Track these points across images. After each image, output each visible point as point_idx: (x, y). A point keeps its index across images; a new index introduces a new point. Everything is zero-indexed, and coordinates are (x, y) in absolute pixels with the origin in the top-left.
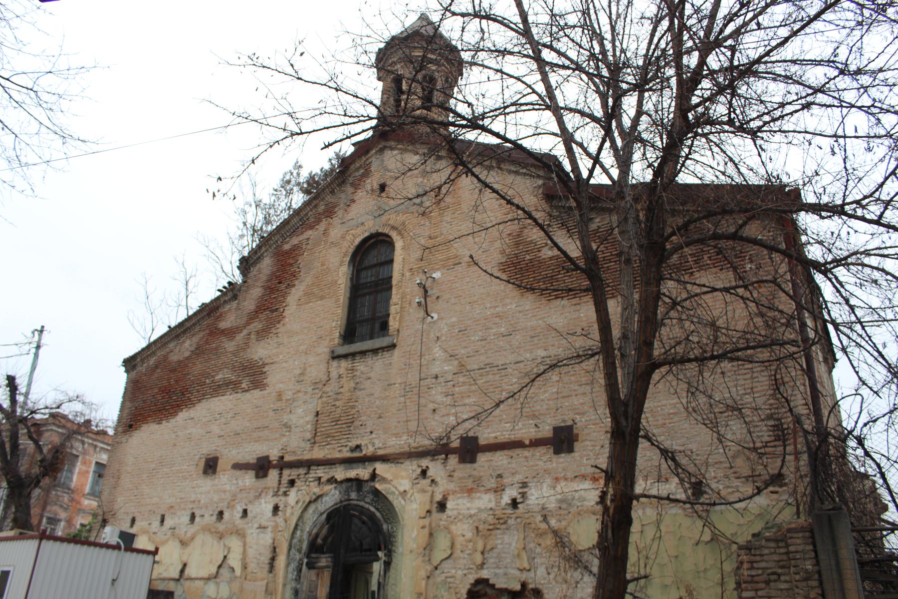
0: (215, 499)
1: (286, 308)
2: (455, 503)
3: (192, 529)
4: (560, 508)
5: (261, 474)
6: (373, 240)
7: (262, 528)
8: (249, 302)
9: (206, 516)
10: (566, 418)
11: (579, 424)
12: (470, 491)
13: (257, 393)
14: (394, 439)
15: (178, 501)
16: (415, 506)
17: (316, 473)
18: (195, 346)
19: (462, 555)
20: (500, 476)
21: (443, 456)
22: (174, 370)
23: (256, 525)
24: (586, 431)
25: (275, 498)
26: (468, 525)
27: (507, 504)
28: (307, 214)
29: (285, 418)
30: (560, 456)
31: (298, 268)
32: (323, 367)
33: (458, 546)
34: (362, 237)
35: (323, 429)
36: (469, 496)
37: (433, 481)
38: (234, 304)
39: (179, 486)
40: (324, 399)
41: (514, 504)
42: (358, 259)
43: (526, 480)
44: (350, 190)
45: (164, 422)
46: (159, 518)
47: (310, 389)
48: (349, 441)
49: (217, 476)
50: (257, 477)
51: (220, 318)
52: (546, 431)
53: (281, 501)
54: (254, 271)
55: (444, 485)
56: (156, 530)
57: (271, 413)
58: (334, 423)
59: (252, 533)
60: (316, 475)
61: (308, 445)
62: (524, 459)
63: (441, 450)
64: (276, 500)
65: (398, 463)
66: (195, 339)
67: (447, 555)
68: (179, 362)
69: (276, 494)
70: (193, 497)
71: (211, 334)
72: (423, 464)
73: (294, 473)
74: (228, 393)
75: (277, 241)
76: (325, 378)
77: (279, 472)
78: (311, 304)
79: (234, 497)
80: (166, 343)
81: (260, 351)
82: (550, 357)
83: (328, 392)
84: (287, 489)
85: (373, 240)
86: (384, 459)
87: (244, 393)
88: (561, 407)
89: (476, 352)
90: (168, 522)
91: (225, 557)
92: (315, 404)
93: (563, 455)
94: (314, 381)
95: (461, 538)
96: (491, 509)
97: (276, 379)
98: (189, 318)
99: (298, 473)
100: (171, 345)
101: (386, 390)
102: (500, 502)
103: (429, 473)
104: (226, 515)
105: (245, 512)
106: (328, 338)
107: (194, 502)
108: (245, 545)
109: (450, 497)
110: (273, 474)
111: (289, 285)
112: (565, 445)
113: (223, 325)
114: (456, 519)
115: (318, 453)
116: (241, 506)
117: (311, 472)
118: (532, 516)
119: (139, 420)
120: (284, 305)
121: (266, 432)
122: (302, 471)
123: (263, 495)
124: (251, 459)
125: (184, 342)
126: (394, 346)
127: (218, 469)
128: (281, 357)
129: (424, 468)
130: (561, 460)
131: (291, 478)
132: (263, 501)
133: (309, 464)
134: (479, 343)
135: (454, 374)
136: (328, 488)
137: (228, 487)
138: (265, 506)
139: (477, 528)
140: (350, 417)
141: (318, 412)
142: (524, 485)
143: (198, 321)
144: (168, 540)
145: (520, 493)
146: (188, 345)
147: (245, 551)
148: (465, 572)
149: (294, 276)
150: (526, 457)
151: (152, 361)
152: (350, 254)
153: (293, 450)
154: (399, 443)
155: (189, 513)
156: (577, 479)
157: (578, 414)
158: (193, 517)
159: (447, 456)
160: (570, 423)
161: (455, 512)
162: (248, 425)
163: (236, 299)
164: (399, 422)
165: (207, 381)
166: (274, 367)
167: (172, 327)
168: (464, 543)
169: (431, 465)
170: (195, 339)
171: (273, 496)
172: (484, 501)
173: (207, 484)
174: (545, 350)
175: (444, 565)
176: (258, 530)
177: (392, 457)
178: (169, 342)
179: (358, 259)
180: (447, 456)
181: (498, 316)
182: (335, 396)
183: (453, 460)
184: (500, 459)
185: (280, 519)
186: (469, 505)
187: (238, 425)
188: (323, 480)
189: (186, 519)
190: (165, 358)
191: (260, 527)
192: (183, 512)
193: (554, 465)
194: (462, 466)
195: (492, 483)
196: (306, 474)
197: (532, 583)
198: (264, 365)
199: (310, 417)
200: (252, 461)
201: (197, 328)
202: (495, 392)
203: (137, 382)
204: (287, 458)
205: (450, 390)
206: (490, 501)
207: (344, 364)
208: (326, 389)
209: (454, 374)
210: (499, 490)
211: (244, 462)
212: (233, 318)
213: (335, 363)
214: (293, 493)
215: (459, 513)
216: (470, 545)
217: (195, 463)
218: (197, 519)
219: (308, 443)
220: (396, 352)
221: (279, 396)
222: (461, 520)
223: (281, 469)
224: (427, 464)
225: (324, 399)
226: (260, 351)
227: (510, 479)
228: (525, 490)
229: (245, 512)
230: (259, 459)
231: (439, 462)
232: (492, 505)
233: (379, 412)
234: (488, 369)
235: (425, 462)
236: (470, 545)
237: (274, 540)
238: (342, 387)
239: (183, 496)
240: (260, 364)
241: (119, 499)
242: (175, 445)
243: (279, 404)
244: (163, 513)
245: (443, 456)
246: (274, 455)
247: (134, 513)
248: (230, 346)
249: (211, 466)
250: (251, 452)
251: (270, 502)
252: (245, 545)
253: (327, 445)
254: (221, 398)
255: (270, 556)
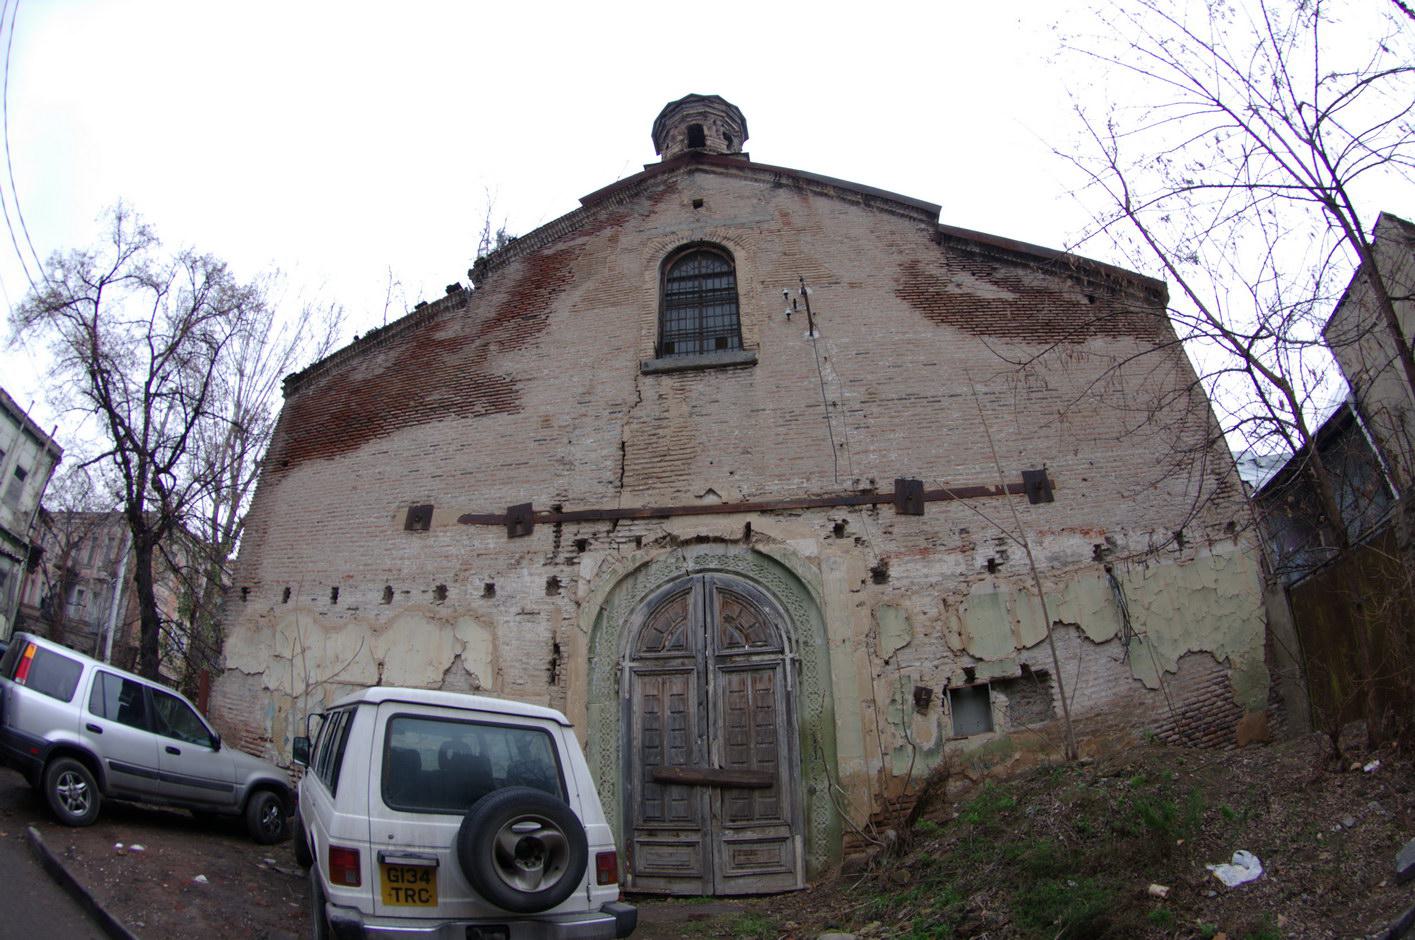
0: (430, 568)
1: (551, 315)
2: (903, 568)
3: (388, 612)
4: (1053, 567)
5: (519, 529)
6: (691, 250)
7: (528, 614)
8: (485, 310)
9: (413, 592)
10: (1034, 462)
11: (1051, 470)
12: (924, 552)
13: (503, 418)
14: (777, 482)
15: (361, 568)
16: (837, 575)
17: (630, 530)
18: (393, 361)
19: (926, 640)
20: (963, 531)
21: (870, 506)
22: (356, 391)
23: (515, 610)
24: (1062, 478)
25: (548, 568)
26: (929, 599)
27: (983, 567)
28: (581, 221)
29: (561, 451)
30: (1038, 505)
31: (570, 273)
32: (629, 385)
33: (919, 630)
34: (678, 244)
35: (636, 467)
36: (924, 558)
37: (857, 540)
38: (461, 312)
39: (363, 546)
40: (634, 426)
41: (992, 566)
42: (669, 267)
43: (1002, 536)
44: (647, 204)
45: (338, 457)
46: (329, 592)
47: (606, 413)
48: (690, 485)
49: (431, 534)
50: (512, 535)
51: (437, 327)
52: (1014, 476)
53: (564, 574)
54: (492, 277)
55: (879, 546)
56: (325, 610)
57: (533, 445)
58: (659, 459)
59: (507, 622)
60: (632, 534)
61: (611, 490)
62: (992, 509)
63: (865, 499)
64: (552, 571)
65: (791, 515)
66: (393, 354)
67: (905, 644)
68: (366, 381)
69: (551, 562)
70: (388, 563)
71: (422, 345)
72: (836, 517)
73: (585, 531)
74: (450, 419)
75: (532, 246)
76: (634, 398)
77: (1184, 343)
78: (596, 311)
79: (466, 567)
80: (348, 359)
81: (504, 365)
82: (994, 393)
83: (641, 417)
84: (574, 554)
85: (691, 250)
86: (764, 510)
87: (478, 418)
88: (1025, 450)
89: (890, 379)
90: (345, 599)
91: (458, 656)
92: (614, 433)
93: (1042, 504)
94: (610, 403)
95: (922, 617)
96: (961, 574)
97: (536, 400)
98: (386, 329)
99: (593, 530)
100: (355, 363)
101: (749, 417)
102: (972, 565)
103: (849, 529)
104: (453, 593)
105: (490, 589)
106: (632, 349)
107: (390, 570)
108: (495, 638)
109: (893, 562)
110: (543, 534)
111: (554, 290)
112: (1042, 492)
113: (440, 335)
114: (909, 592)
115: (627, 501)
116: (481, 580)
117: (618, 528)
118: (1021, 580)
119: (299, 456)
120: (547, 311)
121: (524, 471)
122: (603, 527)
123: (525, 563)
124: (499, 509)
125: (375, 357)
126: (754, 363)
127: (433, 522)
128: (546, 372)
129: (840, 522)
130: (1041, 511)
131: (579, 537)
132: (525, 572)
133: (615, 517)
134: (892, 369)
135: (862, 402)
136: (655, 552)
137: (453, 550)
138: (531, 581)
139: (944, 600)
140: (688, 451)
141: (623, 443)
142: (1001, 541)
143: (401, 331)
144: (346, 625)
145: (998, 552)
146: (381, 361)
147: (495, 647)
148: (936, 663)
149: (564, 281)
150: (995, 507)
151: (323, 382)
152: (661, 259)
153: (582, 497)
154: (786, 487)
155: (383, 586)
156: (1065, 533)
157: (1048, 459)
158: (389, 593)
159: (874, 505)
160: (1040, 468)
161: (905, 582)
162: (488, 460)
163: (463, 307)
164: (781, 459)
165: (412, 403)
166: (531, 384)
167: (361, 337)
168: (928, 623)
169: (850, 518)
170: (393, 354)
171: (545, 565)
172: (948, 565)
173: (414, 545)
174: (986, 385)
175: (901, 656)
176: (518, 618)
177: (780, 506)
178: (353, 357)
179: (669, 267)
180: (874, 505)
181: (909, 342)
182: (657, 423)
183: (887, 512)
184: (958, 509)
185: (563, 601)
186: (925, 571)
187: (469, 461)
188: (644, 541)
189: (378, 596)
190: (343, 377)
191: (523, 612)
192: (371, 585)
193: (1034, 516)
194: (903, 518)
195: (956, 541)
196: (608, 532)
197: (1033, 665)
198: (513, 382)
199: (614, 450)
200: (497, 512)
201: (398, 340)
202: (930, 427)
203: (299, 407)
204: (567, 508)
205: (862, 422)
206: (957, 564)
207: (667, 382)
208: (636, 412)
209: (862, 402)
210: (967, 549)
211: (485, 513)
212: (457, 327)
213: (649, 380)
214: (588, 563)
215: (912, 583)
216: (938, 625)
217: (391, 513)
218: (397, 597)
219: (610, 486)
220: (758, 370)
221: (546, 422)
222: (916, 592)
223: (558, 525)
224: (844, 517)
225: (634, 426)
226: (504, 365)
227: (981, 534)
228: (1003, 548)
229: (490, 589)
230: (511, 510)
231: (865, 514)
232: (962, 568)
233: (742, 445)
234: (913, 400)
235: (840, 514)
236: (938, 625)
237: (555, 632)
238: (667, 411)
239: (369, 562)
240: (508, 380)
241: (265, 561)
242: (355, 488)
243: (546, 433)
244: (336, 585)
245: (870, 506)
246: (542, 503)
247: (287, 582)
248: (451, 359)
249: (419, 518)
250: (499, 498)
251: (540, 575)
252: (495, 638)
253: (648, 489)
254: (437, 424)
255: (550, 658)
